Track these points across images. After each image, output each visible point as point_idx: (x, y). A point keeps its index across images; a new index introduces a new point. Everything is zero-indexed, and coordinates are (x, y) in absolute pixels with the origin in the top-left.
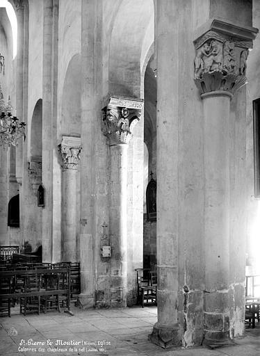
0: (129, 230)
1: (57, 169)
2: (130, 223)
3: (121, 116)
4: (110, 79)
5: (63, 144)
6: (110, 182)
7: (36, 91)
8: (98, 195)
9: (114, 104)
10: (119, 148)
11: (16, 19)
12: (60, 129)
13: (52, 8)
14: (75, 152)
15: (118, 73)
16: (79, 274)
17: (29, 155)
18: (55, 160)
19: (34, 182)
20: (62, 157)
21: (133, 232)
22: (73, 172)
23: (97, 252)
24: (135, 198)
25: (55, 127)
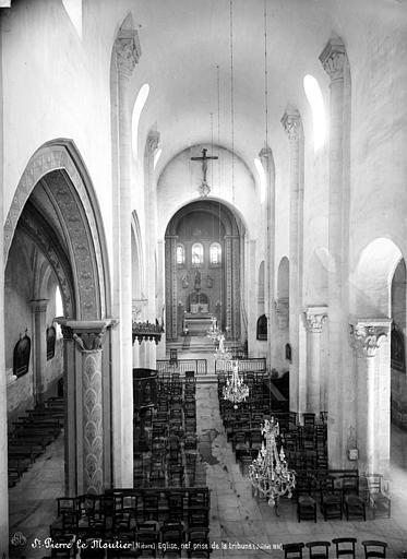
0: (376, 433)
1: (303, 332)
2: (377, 426)
3: (369, 334)
4: (358, 302)
5: (308, 313)
6: (357, 390)
7: (283, 249)
8: (346, 401)
9: (361, 327)
10: (366, 361)
11: (322, 100)
12: (307, 300)
13: (297, 191)
14: (319, 318)
15: (388, 528)
16: (327, 464)
17: (276, 298)
18: (301, 324)
19: (280, 318)
20: (307, 323)
21: (380, 433)
22: (316, 336)
23: (344, 457)
24: (381, 378)
25: (301, 295)
